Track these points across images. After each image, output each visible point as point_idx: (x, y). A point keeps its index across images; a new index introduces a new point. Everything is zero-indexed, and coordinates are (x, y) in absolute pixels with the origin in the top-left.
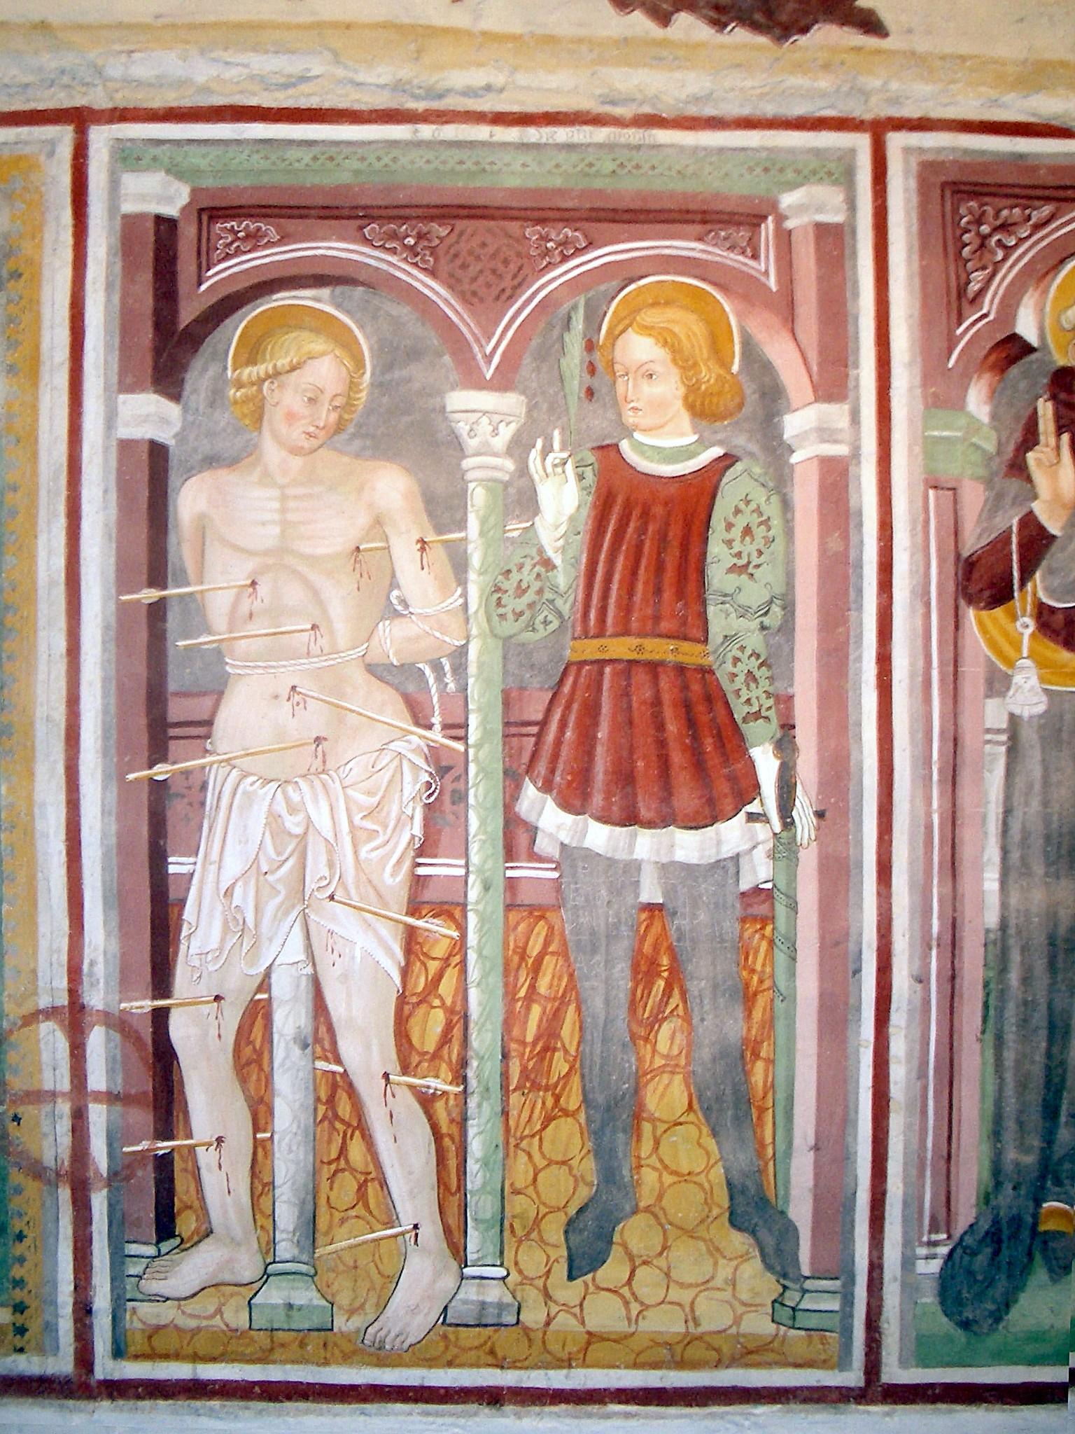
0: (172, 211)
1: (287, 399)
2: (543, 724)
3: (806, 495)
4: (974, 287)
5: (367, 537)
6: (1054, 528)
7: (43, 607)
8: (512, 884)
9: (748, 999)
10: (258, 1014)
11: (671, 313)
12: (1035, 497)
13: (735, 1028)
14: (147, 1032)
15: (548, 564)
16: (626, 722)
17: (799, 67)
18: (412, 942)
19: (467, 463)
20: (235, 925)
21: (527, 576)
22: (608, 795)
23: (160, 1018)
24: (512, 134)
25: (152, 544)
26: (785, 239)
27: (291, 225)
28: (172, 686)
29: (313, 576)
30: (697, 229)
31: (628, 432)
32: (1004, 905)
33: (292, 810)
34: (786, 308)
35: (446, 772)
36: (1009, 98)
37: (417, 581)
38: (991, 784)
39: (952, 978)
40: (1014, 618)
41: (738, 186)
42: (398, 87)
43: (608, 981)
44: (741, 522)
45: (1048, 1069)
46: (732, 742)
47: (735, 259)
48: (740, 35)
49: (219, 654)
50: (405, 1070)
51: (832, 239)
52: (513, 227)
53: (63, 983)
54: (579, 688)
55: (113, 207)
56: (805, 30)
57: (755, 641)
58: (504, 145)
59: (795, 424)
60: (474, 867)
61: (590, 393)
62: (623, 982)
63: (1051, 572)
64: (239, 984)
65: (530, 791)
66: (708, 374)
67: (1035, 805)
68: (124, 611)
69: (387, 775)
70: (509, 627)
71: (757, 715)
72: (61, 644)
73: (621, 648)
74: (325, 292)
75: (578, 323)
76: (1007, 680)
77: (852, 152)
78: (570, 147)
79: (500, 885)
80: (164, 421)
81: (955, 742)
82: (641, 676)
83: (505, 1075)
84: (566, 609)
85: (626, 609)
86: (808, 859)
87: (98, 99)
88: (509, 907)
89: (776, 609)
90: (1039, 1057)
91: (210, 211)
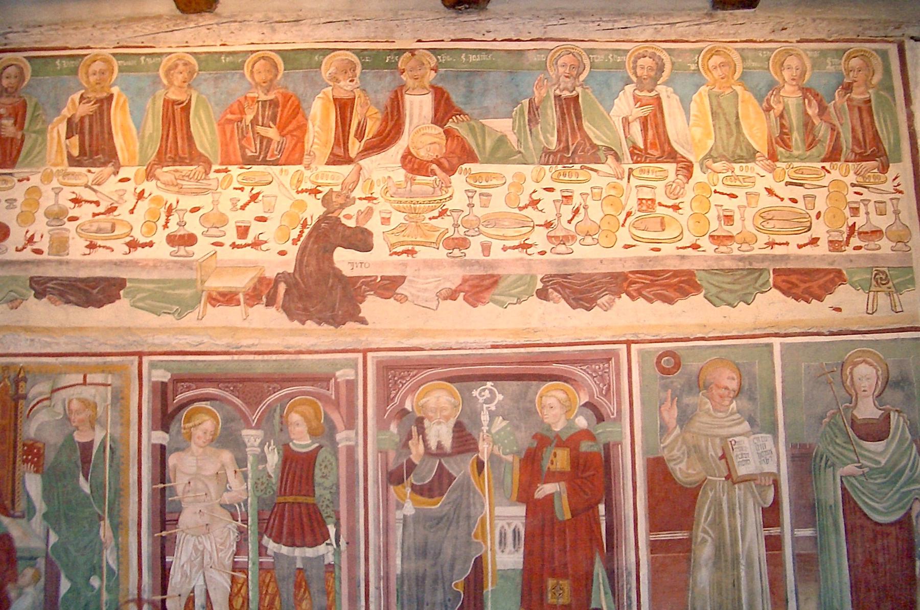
0: (166, 380)
1: (198, 432)
2: (269, 519)
4: (392, 396)
5: (220, 470)
6: (416, 462)
7: (131, 489)
8: (261, 563)
9: (328, 594)
11: (304, 407)
12: (411, 453)
15: (270, 476)
16: (292, 519)
18: (233, 579)
19: (247, 450)
20: (184, 575)
21: (264, 480)
22: (287, 538)
24: (260, 357)
25: (161, 472)
26: (337, 384)
27: (200, 384)
30: (311, 383)
31: (292, 440)
33: (200, 543)
35: (242, 532)
36: (404, 341)
37: (234, 482)
39: (387, 588)
40: (405, 488)
41: (324, 370)
44: (324, 465)
46: (323, 525)
49: (180, 502)
52: (260, 384)
53: (136, 592)
54: (278, 510)
55: (149, 380)
57: (328, 496)
58: (257, 361)
59: (339, 437)
60: (250, 558)
61: (281, 430)
63: (415, 474)
64: (185, 591)
65: (265, 537)
67: (412, 540)
69: (226, 535)
71: (329, 516)
73: (290, 499)
75: (278, 410)
77: (357, 359)
78: (275, 361)
79: (257, 563)
80: (164, 439)
81: (387, 523)
84: (275, 488)
85: (292, 486)
86: (344, 556)
87: (146, 349)
88: (260, 569)
89: (334, 488)
91: (176, 380)
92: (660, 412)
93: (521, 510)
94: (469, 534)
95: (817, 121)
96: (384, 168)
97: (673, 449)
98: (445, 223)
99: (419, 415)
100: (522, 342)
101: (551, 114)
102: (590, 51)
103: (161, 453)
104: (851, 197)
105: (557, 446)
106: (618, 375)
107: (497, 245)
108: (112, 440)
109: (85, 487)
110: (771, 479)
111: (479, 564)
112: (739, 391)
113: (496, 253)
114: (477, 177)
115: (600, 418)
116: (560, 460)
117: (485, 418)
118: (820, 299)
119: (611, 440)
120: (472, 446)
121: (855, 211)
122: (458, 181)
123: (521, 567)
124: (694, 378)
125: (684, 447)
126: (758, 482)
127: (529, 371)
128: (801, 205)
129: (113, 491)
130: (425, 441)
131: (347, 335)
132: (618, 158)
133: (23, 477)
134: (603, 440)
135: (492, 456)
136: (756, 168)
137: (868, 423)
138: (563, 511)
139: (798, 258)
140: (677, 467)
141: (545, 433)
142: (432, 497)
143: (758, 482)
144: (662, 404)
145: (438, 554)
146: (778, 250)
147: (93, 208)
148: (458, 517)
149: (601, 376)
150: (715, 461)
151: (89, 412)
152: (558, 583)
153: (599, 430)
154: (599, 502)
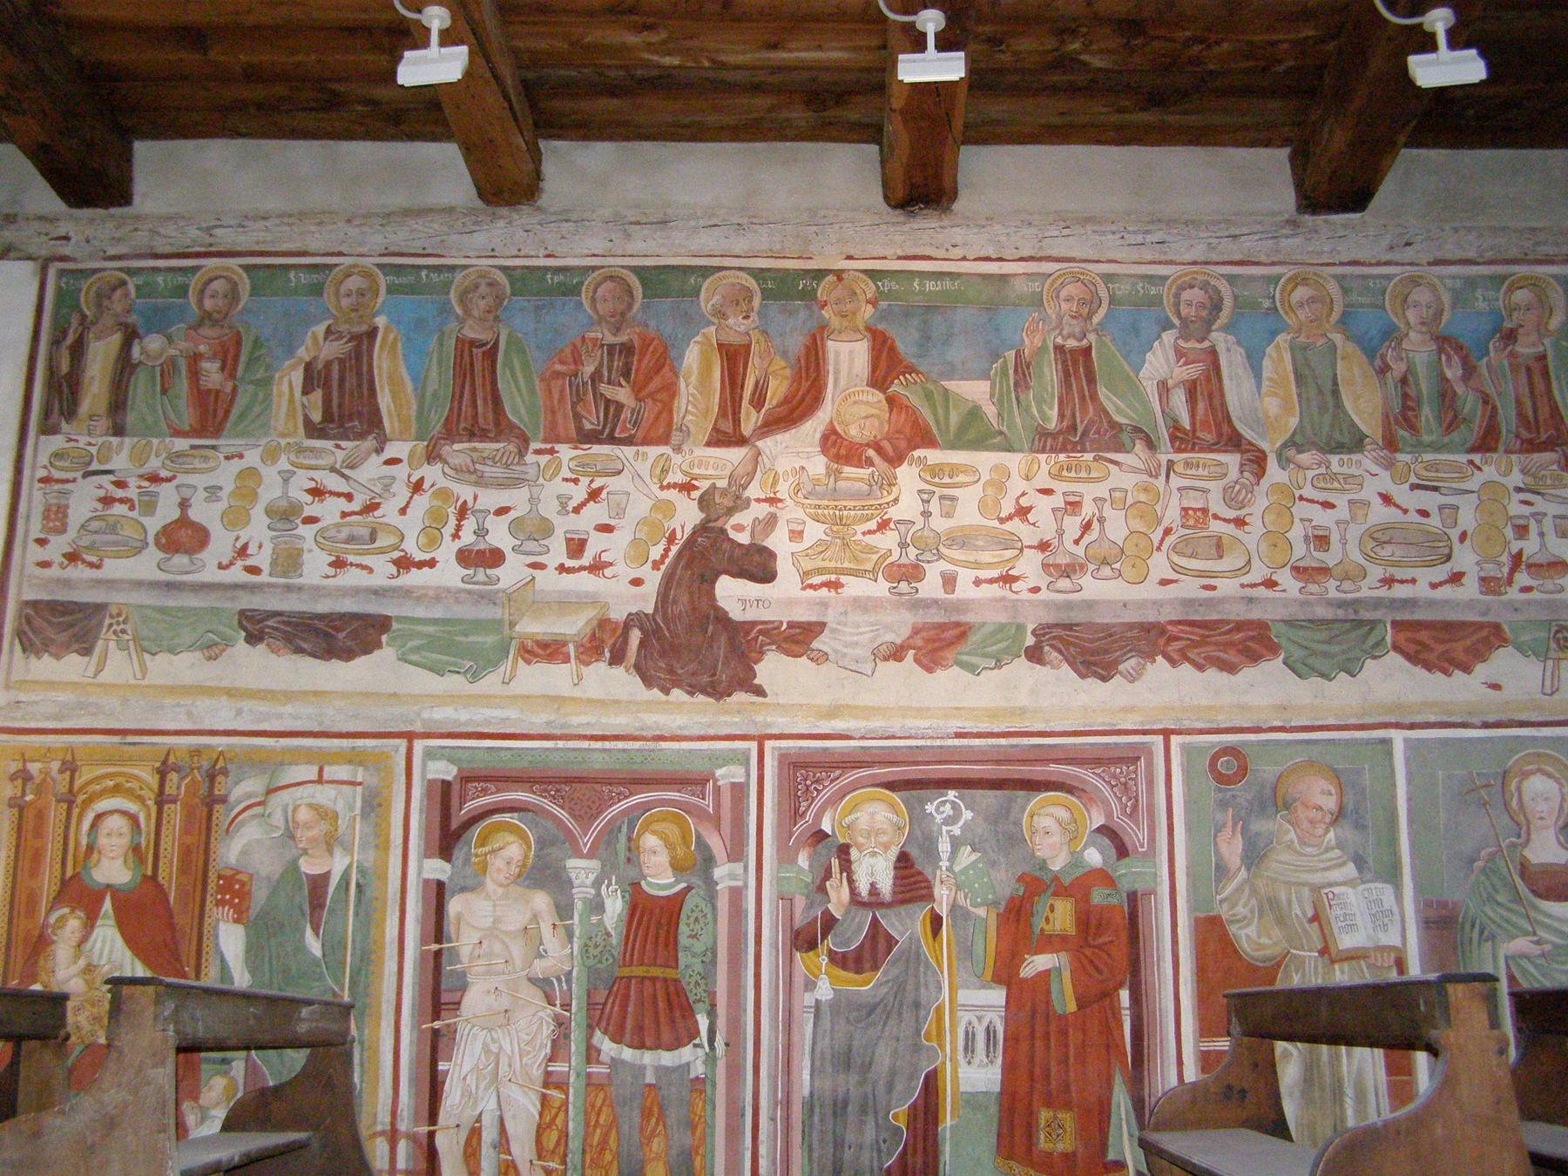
0: (449, 778)
1: (497, 862)
2: (605, 1004)
3: (723, 903)
8: (589, 1075)
9: (693, 1126)
10: (475, 1133)
11: (664, 825)
13: (687, 1140)
14: (425, 1141)
15: (608, 934)
17: (726, 712)
18: (544, 1099)
20: (467, 1093)
21: (599, 940)
23: (431, 1135)
24: (599, 745)
25: (437, 926)
26: (717, 789)
28: (443, 987)
29: (507, 940)
32: (812, 1085)
34: (716, 821)
35: (561, 1024)
38: (806, 1028)
41: (698, 766)
42: (549, 723)
43: (631, 1118)
45: (834, 1163)
46: (689, 1013)
47: (694, 800)
48: (701, 698)
50: (540, 1157)
51: (739, 790)
52: (597, 787)
53: (388, 1119)
54: (620, 988)
56: (729, 695)
57: (699, 968)
59: (718, 873)
60: (571, 1067)
62: (637, 1120)
64: (468, 1118)
65: (598, 1033)
66: (680, 851)
67: (827, 1040)
68: (423, 955)
70: (591, 962)
72: (395, 968)
73: (639, 971)
74: (516, 815)
76: (815, 984)
81: (789, 1012)
82: (648, 983)
83: (583, 1161)
85: (643, 953)
86: (721, 1066)
87: (418, 727)
90: (830, 1156)
91: (466, 778)
92: (1216, 844)
93: (997, 996)
94: (918, 1032)
95: (1460, 389)
96: (794, 454)
97: (1234, 905)
98: (888, 540)
99: (842, 841)
100: (1003, 728)
101: (1050, 374)
102: (1108, 278)
103: (438, 894)
104: (1515, 509)
105: (1055, 894)
106: (1150, 783)
107: (965, 577)
108: (362, 872)
109: (314, 946)
110: (1393, 955)
111: (932, 1084)
112: (1339, 815)
113: (965, 589)
114: (936, 470)
115: (1122, 851)
116: (1060, 916)
117: (944, 847)
118: (1467, 669)
119: (1139, 887)
120: (924, 892)
121: (1522, 531)
122: (907, 475)
123: (997, 1088)
124: (1268, 792)
125: (1254, 902)
126: (1372, 961)
127: (1010, 776)
128: (1435, 521)
129: (358, 952)
130: (851, 881)
131: (735, 713)
132: (1151, 445)
133: (216, 928)
134: (1125, 886)
135: (954, 907)
136: (1366, 462)
137: (1547, 870)
138: (1065, 1000)
139: (1431, 603)
140: (1243, 933)
141: (1038, 874)
142: (859, 971)
143: (1372, 961)
144: (1218, 831)
145: (867, 1067)
146: (1400, 592)
147: (342, 504)
148: (901, 1005)
149: (1125, 784)
150: (1301, 924)
151: (324, 827)
152: (1055, 1117)
153: (1122, 869)
154: (1120, 985)
